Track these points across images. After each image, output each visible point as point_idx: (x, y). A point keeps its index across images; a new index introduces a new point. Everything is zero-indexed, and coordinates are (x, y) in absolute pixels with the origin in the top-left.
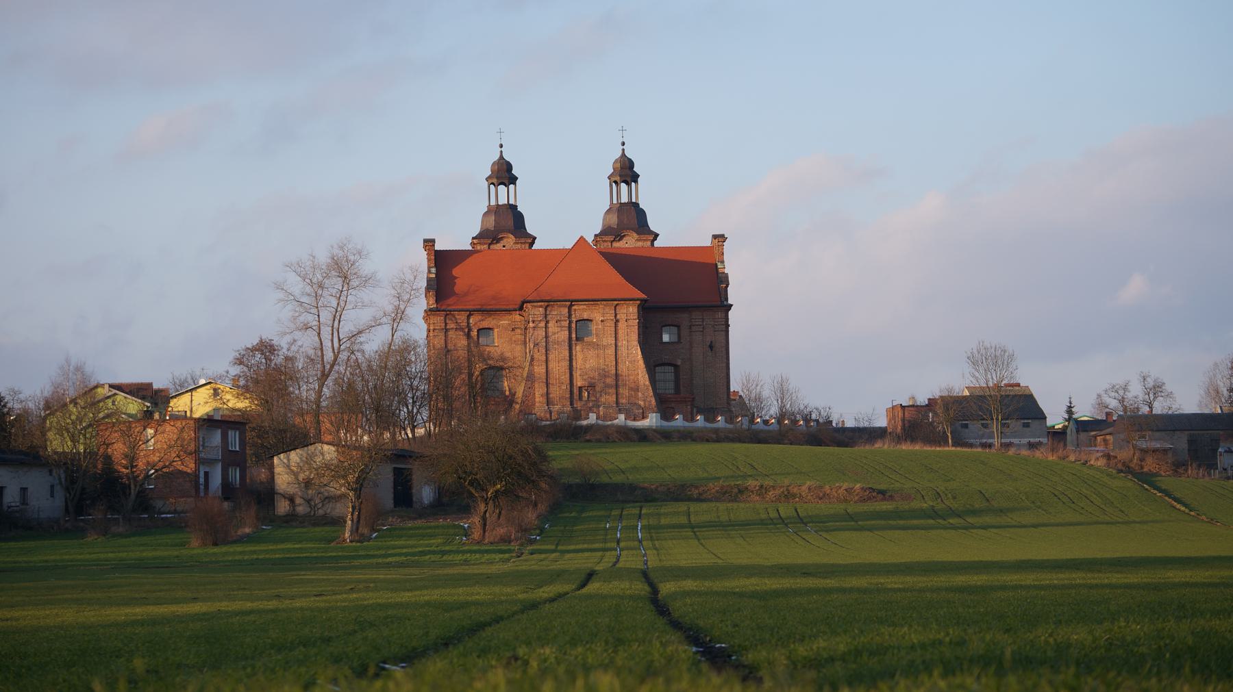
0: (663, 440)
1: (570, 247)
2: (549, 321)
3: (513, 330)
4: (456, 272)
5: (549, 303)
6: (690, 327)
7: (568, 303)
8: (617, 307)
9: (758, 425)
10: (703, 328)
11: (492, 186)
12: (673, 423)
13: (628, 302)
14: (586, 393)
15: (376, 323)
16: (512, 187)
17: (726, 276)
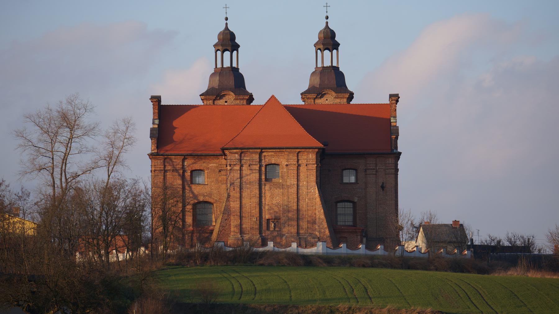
0: (324, 264)
1: (263, 103)
2: (243, 165)
3: (220, 171)
4: (175, 123)
5: (243, 150)
6: (366, 170)
7: (259, 151)
8: (299, 154)
9: (414, 253)
10: (376, 171)
11: (319, 51)
12: (337, 251)
13: (308, 150)
14: (273, 224)
15: (95, 166)
16: (335, 51)
17: (397, 129)
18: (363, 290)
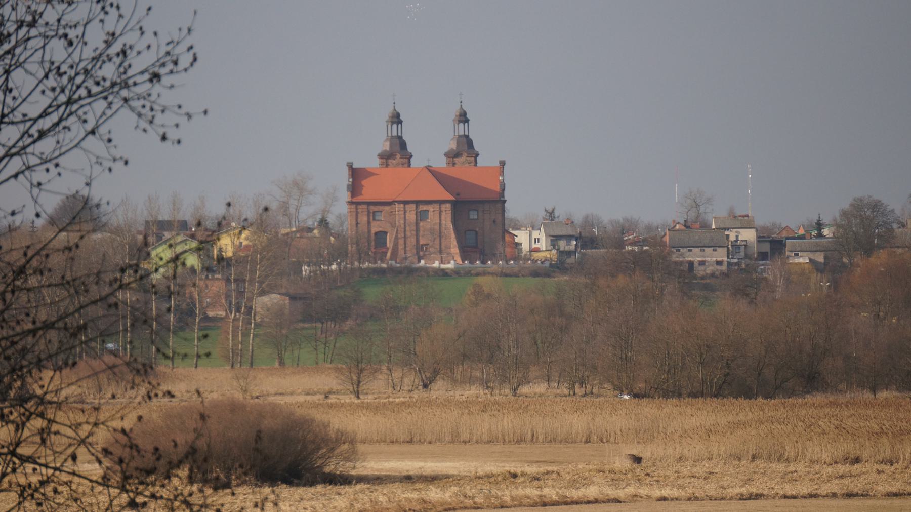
4: (364, 182)
6: (483, 211)
18: (18, 264)
